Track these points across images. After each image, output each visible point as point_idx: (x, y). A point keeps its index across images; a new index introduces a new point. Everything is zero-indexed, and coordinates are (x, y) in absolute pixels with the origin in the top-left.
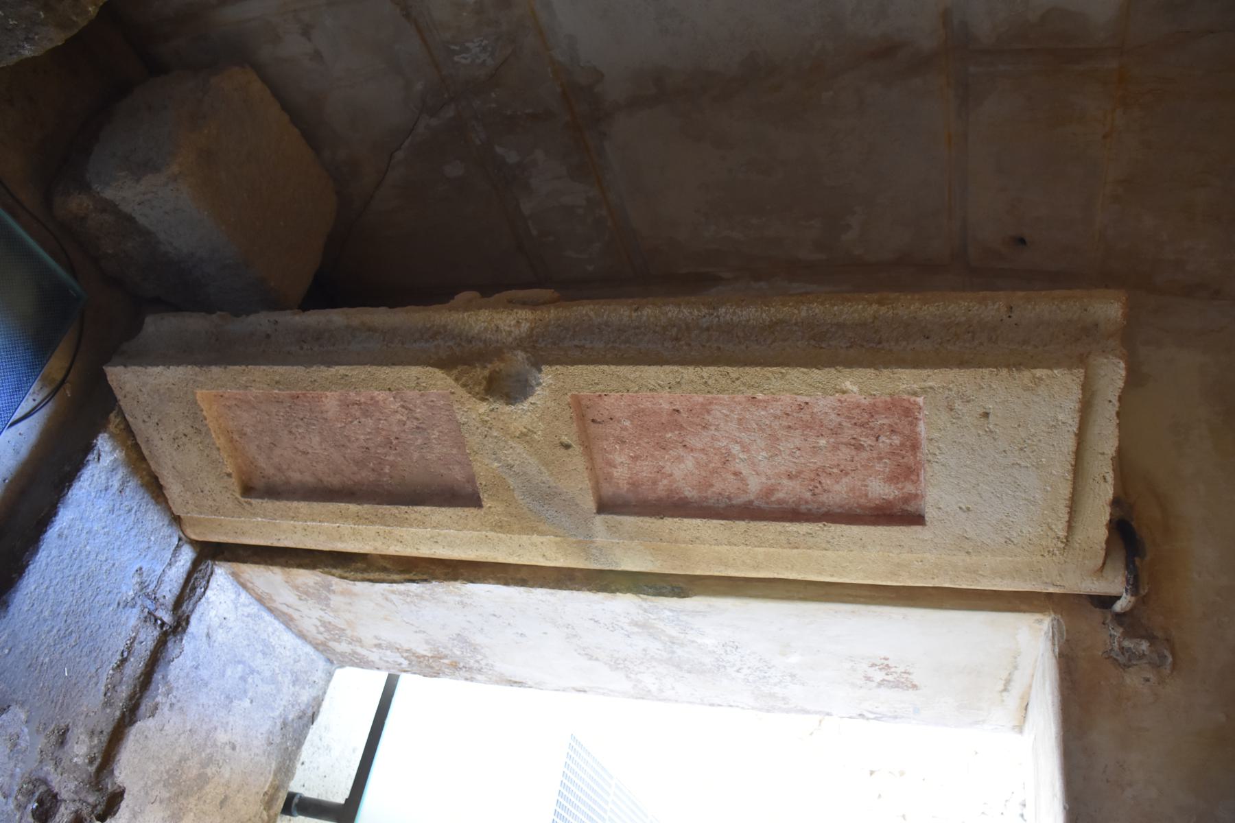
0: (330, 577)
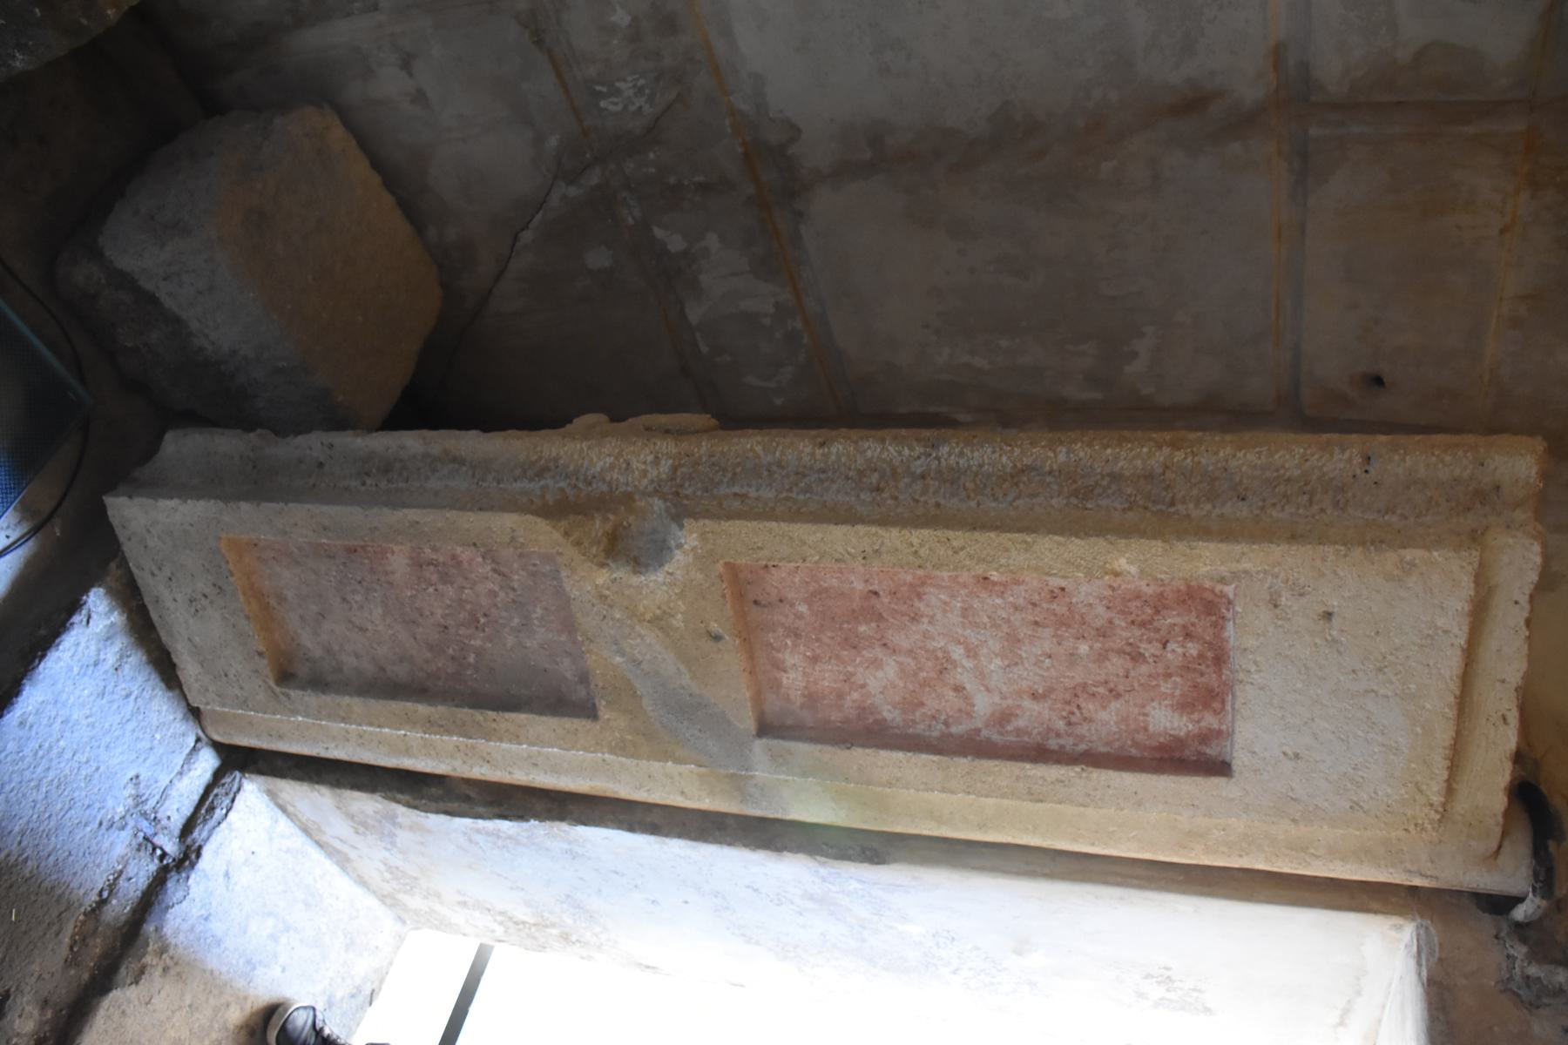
0: (394, 805)
